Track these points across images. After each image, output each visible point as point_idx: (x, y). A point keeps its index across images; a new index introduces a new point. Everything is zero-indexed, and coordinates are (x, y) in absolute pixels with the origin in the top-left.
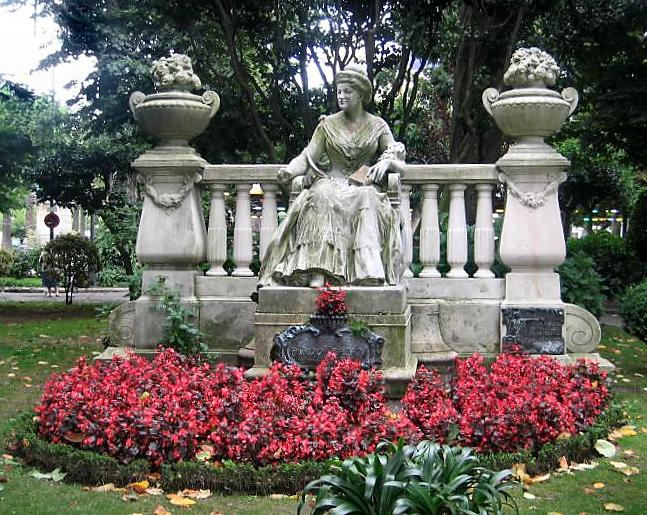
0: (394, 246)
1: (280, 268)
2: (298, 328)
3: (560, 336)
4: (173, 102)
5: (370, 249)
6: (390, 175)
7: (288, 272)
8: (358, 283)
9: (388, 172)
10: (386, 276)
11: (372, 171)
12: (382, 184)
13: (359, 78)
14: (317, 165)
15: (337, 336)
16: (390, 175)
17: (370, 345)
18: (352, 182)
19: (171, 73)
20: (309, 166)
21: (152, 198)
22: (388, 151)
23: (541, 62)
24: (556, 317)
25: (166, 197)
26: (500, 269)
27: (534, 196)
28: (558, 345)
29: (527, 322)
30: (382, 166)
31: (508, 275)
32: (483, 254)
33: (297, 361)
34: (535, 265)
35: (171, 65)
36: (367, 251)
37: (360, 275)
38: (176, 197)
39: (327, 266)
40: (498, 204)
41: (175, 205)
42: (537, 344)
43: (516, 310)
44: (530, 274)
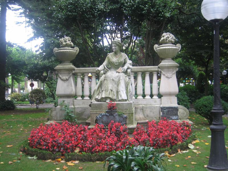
0: (129, 90)
1: (97, 97)
2: (103, 114)
3: (177, 115)
4: (66, 50)
5: (123, 91)
6: (128, 70)
7: (99, 98)
8: (119, 101)
9: (127, 69)
10: (127, 98)
11: (123, 69)
12: (126, 72)
13: (118, 42)
14: (107, 67)
15: (114, 116)
16: (128, 70)
17: (123, 118)
18: (117, 72)
19: (65, 42)
20: (105, 68)
21: (60, 78)
22: (127, 63)
23: (170, 37)
24: (176, 109)
25: (64, 77)
26: (160, 96)
27: (169, 75)
28: (177, 117)
29: (168, 111)
30: (125, 67)
31: (162, 98)
32: (155, 92)
33: (103, 123)
34: (170, 94)
35: (65, 40)
36: (122, 91)
37: (120, 98)
38: (67, 77)
39: (110, 96)
40: (159, 77)
41: (67, 80)
42: (171, 117)
43: (165, 107)
44: (168, 97)
